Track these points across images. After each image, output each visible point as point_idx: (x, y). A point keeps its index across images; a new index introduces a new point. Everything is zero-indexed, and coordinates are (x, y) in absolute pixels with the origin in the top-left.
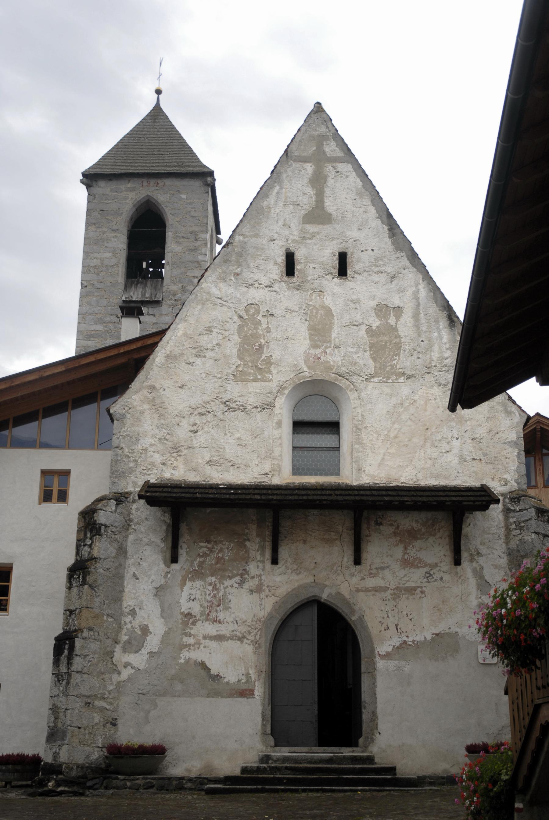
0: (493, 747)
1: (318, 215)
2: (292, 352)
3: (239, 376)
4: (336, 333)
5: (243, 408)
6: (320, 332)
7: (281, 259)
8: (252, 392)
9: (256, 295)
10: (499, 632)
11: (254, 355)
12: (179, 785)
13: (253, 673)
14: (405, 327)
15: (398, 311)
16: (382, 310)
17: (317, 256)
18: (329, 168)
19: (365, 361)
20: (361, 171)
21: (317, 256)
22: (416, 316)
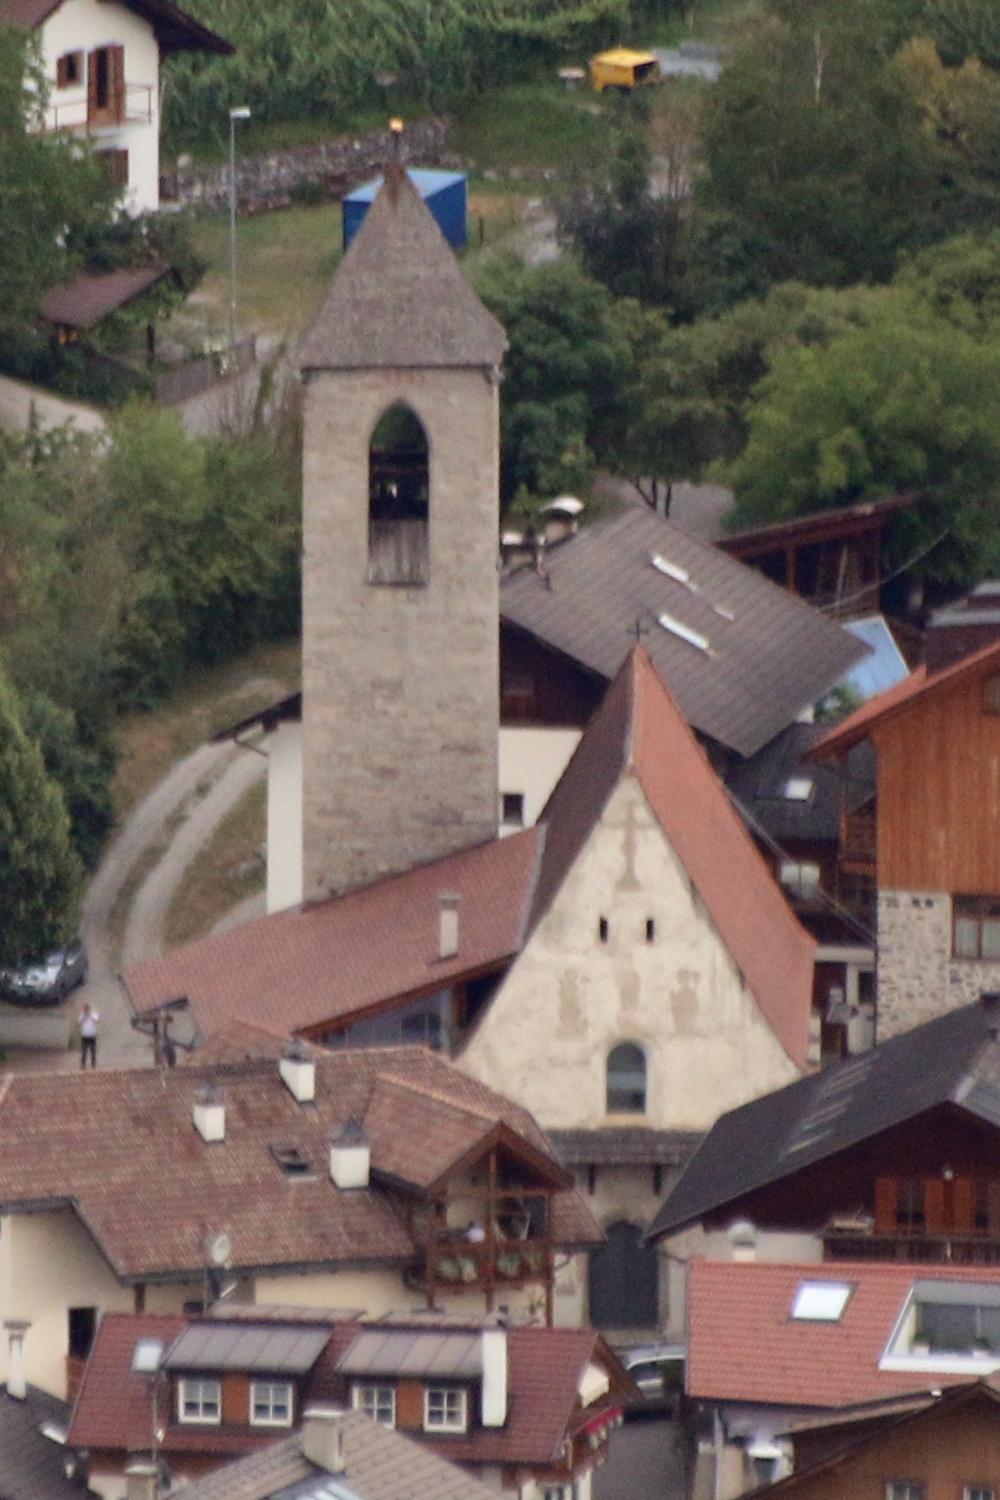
0: (226, 1260)
1: (628, 881)
2: (605, 1019)
3: (561, 1034)
4: (644, 996)
5: (564, 1064)
6: (629, 993)
7: (596, 926)
8: (572, 1048)
9: (574, 960)
10: (244, 112)
11: (572, 1015)
12: (70, 1397)
13: (574, 1278)
14: (702, 991)
15: (697, 976)
16: (684, 974)
17: (627, 923)
18: (639, 836)
19: (668, 1021)
20: (808, 1323)
21: (627, 923)
22: (712, 982)
